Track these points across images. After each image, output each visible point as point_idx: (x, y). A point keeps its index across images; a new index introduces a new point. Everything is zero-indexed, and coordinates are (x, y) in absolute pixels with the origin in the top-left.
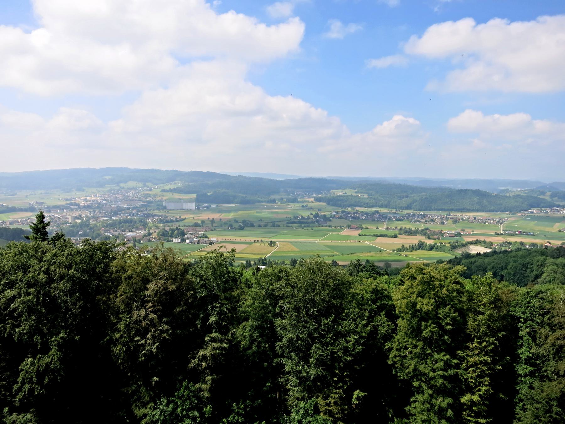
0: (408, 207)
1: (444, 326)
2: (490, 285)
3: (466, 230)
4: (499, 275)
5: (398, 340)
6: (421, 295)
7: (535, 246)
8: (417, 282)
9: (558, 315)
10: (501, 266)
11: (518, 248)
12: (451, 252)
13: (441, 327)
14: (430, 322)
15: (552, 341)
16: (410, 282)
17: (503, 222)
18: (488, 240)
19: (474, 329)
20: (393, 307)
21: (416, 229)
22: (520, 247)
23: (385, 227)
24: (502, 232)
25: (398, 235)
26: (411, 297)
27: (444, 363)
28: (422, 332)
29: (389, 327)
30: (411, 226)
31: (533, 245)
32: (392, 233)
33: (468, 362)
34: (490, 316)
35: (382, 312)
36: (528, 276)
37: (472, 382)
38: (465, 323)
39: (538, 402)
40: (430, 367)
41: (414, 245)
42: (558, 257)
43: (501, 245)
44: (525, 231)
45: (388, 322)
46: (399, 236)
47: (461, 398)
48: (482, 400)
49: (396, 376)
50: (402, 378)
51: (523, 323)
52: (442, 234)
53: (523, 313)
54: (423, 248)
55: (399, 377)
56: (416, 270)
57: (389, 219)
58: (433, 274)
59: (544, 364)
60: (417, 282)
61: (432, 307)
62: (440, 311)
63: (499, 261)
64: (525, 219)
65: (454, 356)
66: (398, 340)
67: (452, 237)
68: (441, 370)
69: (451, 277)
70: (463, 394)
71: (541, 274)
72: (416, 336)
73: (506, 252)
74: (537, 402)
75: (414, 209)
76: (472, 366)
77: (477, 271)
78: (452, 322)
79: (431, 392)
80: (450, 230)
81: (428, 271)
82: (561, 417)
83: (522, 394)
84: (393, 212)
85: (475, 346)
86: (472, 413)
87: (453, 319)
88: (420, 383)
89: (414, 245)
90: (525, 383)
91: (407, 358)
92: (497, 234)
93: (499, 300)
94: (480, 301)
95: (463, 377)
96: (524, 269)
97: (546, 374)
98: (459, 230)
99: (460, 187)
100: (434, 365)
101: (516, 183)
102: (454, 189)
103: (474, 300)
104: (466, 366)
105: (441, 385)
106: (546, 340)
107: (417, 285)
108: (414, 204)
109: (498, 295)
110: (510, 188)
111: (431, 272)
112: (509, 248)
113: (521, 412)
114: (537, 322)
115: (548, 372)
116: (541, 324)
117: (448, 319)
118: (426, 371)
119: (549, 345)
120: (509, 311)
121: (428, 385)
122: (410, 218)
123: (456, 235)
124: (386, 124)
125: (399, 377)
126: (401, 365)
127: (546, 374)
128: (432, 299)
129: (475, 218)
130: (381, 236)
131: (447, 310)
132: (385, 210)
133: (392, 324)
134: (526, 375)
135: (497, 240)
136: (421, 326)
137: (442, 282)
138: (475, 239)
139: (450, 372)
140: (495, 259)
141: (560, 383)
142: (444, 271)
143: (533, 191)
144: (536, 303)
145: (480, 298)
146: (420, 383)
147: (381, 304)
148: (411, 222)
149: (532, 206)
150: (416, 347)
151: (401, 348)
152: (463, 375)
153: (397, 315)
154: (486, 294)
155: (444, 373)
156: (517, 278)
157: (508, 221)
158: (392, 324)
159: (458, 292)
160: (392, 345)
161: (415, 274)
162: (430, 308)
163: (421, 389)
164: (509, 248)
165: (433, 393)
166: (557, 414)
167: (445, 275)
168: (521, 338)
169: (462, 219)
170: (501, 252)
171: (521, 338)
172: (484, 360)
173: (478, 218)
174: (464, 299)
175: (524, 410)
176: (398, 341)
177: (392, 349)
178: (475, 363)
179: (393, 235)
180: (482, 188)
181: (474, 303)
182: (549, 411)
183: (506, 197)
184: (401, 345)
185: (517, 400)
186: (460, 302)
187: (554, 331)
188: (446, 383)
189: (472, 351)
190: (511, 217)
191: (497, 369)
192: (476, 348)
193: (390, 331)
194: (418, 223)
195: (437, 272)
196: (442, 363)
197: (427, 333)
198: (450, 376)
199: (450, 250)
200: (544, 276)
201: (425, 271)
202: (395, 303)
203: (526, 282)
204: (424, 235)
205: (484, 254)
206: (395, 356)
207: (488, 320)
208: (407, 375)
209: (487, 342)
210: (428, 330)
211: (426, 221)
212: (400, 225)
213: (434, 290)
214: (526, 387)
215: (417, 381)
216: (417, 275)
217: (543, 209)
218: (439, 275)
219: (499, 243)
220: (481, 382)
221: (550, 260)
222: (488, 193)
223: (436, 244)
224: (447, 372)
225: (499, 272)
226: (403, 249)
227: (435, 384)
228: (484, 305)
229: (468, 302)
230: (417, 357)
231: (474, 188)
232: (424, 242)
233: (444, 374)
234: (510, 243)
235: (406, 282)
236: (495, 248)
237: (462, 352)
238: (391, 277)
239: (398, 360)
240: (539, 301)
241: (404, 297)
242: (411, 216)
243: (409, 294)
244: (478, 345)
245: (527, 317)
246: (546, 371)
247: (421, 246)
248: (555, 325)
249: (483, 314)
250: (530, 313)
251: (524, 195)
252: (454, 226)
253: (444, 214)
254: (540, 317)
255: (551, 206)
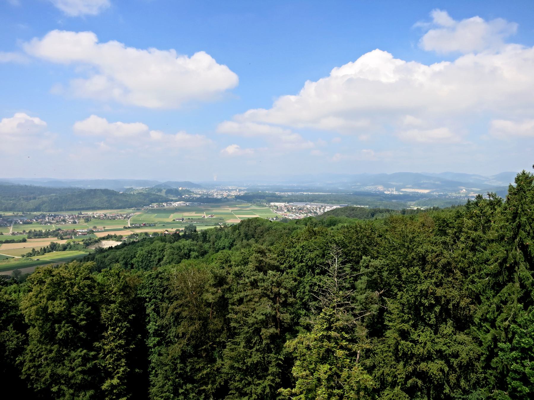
0: (37, 209)
1: (78, 323)
2: (118, 275)
3: (97, 227)
4: (130, 264)
5: (31, 350)
6: (51, 298)
7: (156, 235)
8: (46, 285)
9: (174, 290)
10: (130, 256)
11: (144, 238)
12: (85, 249)
13: (75, 325)
14: (64, 322)
15: (171, 312)
16: (38, 287)
17: (130, 216)
18: (118, 233)
19: (107, 319)
20: (22, 316)
21: (47, 230)
22: (145, 237)
23: (11, 232)
24: (129, 226)
25: (26, 239)
26: (41, 302)
27: (82, 359)
28: (56, 335)
29: (18, 339)
30: (43, 229)
31: (155, 234)
32: (21, 237)
33: (105, 350)
34: (121, 303)
35: (9, 325)
36: (153, 261)
37: (110, 368)
38: (99, 314)
39: (166, 365)
40: (68, 366)
41: (46, 247)
42: (174, 242)
43: (129, 238)
44: (148, 223)
45: (17, 334)
46: (28, 240)
47: (102, 386)
48: (121, 381)
49: (32, 389)
50: (39, 388)
51: (149, 302)
52: (74, 233)
53: (148, 293)
54: (56, 249)
55: (35, 389)
56: (44, 274)
57: (16, 223)
58: (62, 274)
59: (167, 332)
60: (46, 285)
61: (65, 307)
62: (73, 309)
63: (129, 252)
64: (147, 213)
65: (91, 349)
66: (31, 350)
67: (84, 235)
68: (79, 366)
69: (81, 274)
70: (103, 382)
71: (163, 257)
72: (51, 341)
73: (134, 243)
74: (165, 365)
75: (43, 211)
76: (108, 353)
77: (110, 263)
78: (86, 317)
79: (71, 391)
80: (82, 228)
81: (57, 272)
82: (184, 371)
83: (153, 362)
84: (20, 216)
85: (110, 333)
86: (113, 396)
87: (87, 314)
88: (60, 386)
89: (46, 247)
90: (155, 353)
91: (43, 366)
92: (125, 228)
93: (128, 286)
94: (111, 291)
95: (102, 366)
96: (149, 255)
97: (169, 339)
98: (91, 228)
99: (89, 187)
100: (72, 364)
101: (139, 183)
102: (84, 189)
103: (105, 292)
104: (103, 354)
105: (81, 380)
106: (167, 312)
107: (47, 288)
108: (44, 206)
109: (126, 282)
110: (134, 187)
111: (61, 272)
112: (136, 239)
113: (154, 378)
114: (159, 299)
115: (171, 337)
116: (162, 300)
117: (82, 315)
118: (65, 372)
119: (169, 316)
120: (136, 295)
121: (68, 385)
122: (41, 219)
123: (88, 233)
124: (5, 121)
125: (35, 389)
126: (37, 375)
127: (169, 339)
128: (64, 299)
129: (105, 215)
130: (7, 242)
131: (80, 306)
132: (10, 214)
133: (22, 336)
134: (155, 346)
135: (126, 233)
136: (55, 329)
137: (73, 281)
138: (107, 235)
139: (89, 365)
140: (125, 250)
141: (180, 344)
142: (74, 269)
143: (152, 189)
144: (157, 282)
145: (111, 288)
146: (60, 386)
147: (7, 317)
148: (41, 224)
149: (152, 202)
150: (51, 351)
151: (35, 357)
152: (101, 364)
153: (27, 324)
154: (115, 284)
155: (83, 368)
156: (144, 264)
157: (133, 216)
158: (22, 336)
159: (89, 287)
160: (24, 357)
161: (43, 278)
162: (63, 309)
163: (62, 392)
164: (136, 239)
165: (74, 391)
166: (181, 369)
167: (76, 273)
168: (148, 315)
169: (94, 217)
170: (130, 243)
171: (148, 315)
172: (119, 344)
173: (108, 215)
174: (96, 292)
175: (156, 375)
176: (31, 352)
177: (25, 361)
178: (111, 349)
179: (21, 239)
180: (110, 187)
181: (105, 294)
182: (175, 369)
183: (131, 194)
184: (34, 355)
185: (150, 369)
186: (93, 296)
187: (172, 303)
188: (86, 377)
189: (107, 339)
190: (135, 212)
191: (131, 349)
192: (111, 335)
193: (21, 343)
194: (49, 224)
195: (67, 271)
196: (80, 360)
197: (62, 334)
198: (90, 368)
199: (83, 248)
200: (165, 258)
201: (54, 273)
202: (23, 312)
203: (152, 266)
204: (56, 236)
205: (116, 247)
206: (29, 369)
207: (120, 307)
208: (44, 383)
209: (119, 327)
210: (62, 331)
211: (57, 222)
212: (28, 228)
213: (65, 290)
214: (156, 356)
215: (56, 386)
216: (45, 278)
217: (161, 204)
218: (69, 274)
219: (128, 236)
220: (119, 365)
221: (168, 245)
222: (115, 192)
223: (69, 244)
224: (85, 366)
225: (130, 261)
226: (34, 252)
227: (76, 381)
228: (115, 294)
229: (100, 295)
230: (54, 361)
231: (103, 187)
232: (57, 243)
233: (83, 369)
234: (137, 235)
235: (34, 287)
236: (125, 241)
237: (98, 343)
238: (21, 285)
239: (33, 372)
240: (159, 281)
241: (33, 304)
242: (41, 218)
243: (38, 299)
244: (112, 332)
245: (151, 296)
246: (169, 337)
247: (53, 247)
248: (173, 298)
249: (114, 302)
250: (153, 293)
251: (146, 192)
252: (86, 224)
253: (76, 213)
254: (161, 294)
255: (167, 201)
